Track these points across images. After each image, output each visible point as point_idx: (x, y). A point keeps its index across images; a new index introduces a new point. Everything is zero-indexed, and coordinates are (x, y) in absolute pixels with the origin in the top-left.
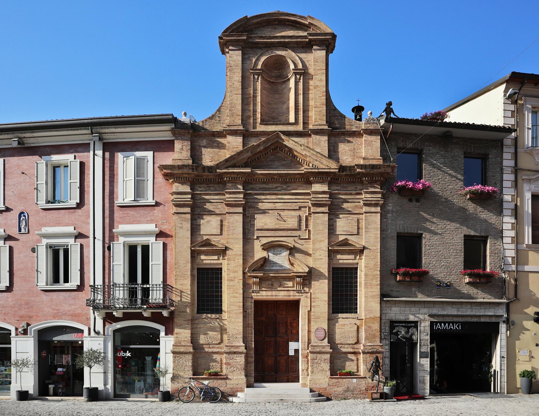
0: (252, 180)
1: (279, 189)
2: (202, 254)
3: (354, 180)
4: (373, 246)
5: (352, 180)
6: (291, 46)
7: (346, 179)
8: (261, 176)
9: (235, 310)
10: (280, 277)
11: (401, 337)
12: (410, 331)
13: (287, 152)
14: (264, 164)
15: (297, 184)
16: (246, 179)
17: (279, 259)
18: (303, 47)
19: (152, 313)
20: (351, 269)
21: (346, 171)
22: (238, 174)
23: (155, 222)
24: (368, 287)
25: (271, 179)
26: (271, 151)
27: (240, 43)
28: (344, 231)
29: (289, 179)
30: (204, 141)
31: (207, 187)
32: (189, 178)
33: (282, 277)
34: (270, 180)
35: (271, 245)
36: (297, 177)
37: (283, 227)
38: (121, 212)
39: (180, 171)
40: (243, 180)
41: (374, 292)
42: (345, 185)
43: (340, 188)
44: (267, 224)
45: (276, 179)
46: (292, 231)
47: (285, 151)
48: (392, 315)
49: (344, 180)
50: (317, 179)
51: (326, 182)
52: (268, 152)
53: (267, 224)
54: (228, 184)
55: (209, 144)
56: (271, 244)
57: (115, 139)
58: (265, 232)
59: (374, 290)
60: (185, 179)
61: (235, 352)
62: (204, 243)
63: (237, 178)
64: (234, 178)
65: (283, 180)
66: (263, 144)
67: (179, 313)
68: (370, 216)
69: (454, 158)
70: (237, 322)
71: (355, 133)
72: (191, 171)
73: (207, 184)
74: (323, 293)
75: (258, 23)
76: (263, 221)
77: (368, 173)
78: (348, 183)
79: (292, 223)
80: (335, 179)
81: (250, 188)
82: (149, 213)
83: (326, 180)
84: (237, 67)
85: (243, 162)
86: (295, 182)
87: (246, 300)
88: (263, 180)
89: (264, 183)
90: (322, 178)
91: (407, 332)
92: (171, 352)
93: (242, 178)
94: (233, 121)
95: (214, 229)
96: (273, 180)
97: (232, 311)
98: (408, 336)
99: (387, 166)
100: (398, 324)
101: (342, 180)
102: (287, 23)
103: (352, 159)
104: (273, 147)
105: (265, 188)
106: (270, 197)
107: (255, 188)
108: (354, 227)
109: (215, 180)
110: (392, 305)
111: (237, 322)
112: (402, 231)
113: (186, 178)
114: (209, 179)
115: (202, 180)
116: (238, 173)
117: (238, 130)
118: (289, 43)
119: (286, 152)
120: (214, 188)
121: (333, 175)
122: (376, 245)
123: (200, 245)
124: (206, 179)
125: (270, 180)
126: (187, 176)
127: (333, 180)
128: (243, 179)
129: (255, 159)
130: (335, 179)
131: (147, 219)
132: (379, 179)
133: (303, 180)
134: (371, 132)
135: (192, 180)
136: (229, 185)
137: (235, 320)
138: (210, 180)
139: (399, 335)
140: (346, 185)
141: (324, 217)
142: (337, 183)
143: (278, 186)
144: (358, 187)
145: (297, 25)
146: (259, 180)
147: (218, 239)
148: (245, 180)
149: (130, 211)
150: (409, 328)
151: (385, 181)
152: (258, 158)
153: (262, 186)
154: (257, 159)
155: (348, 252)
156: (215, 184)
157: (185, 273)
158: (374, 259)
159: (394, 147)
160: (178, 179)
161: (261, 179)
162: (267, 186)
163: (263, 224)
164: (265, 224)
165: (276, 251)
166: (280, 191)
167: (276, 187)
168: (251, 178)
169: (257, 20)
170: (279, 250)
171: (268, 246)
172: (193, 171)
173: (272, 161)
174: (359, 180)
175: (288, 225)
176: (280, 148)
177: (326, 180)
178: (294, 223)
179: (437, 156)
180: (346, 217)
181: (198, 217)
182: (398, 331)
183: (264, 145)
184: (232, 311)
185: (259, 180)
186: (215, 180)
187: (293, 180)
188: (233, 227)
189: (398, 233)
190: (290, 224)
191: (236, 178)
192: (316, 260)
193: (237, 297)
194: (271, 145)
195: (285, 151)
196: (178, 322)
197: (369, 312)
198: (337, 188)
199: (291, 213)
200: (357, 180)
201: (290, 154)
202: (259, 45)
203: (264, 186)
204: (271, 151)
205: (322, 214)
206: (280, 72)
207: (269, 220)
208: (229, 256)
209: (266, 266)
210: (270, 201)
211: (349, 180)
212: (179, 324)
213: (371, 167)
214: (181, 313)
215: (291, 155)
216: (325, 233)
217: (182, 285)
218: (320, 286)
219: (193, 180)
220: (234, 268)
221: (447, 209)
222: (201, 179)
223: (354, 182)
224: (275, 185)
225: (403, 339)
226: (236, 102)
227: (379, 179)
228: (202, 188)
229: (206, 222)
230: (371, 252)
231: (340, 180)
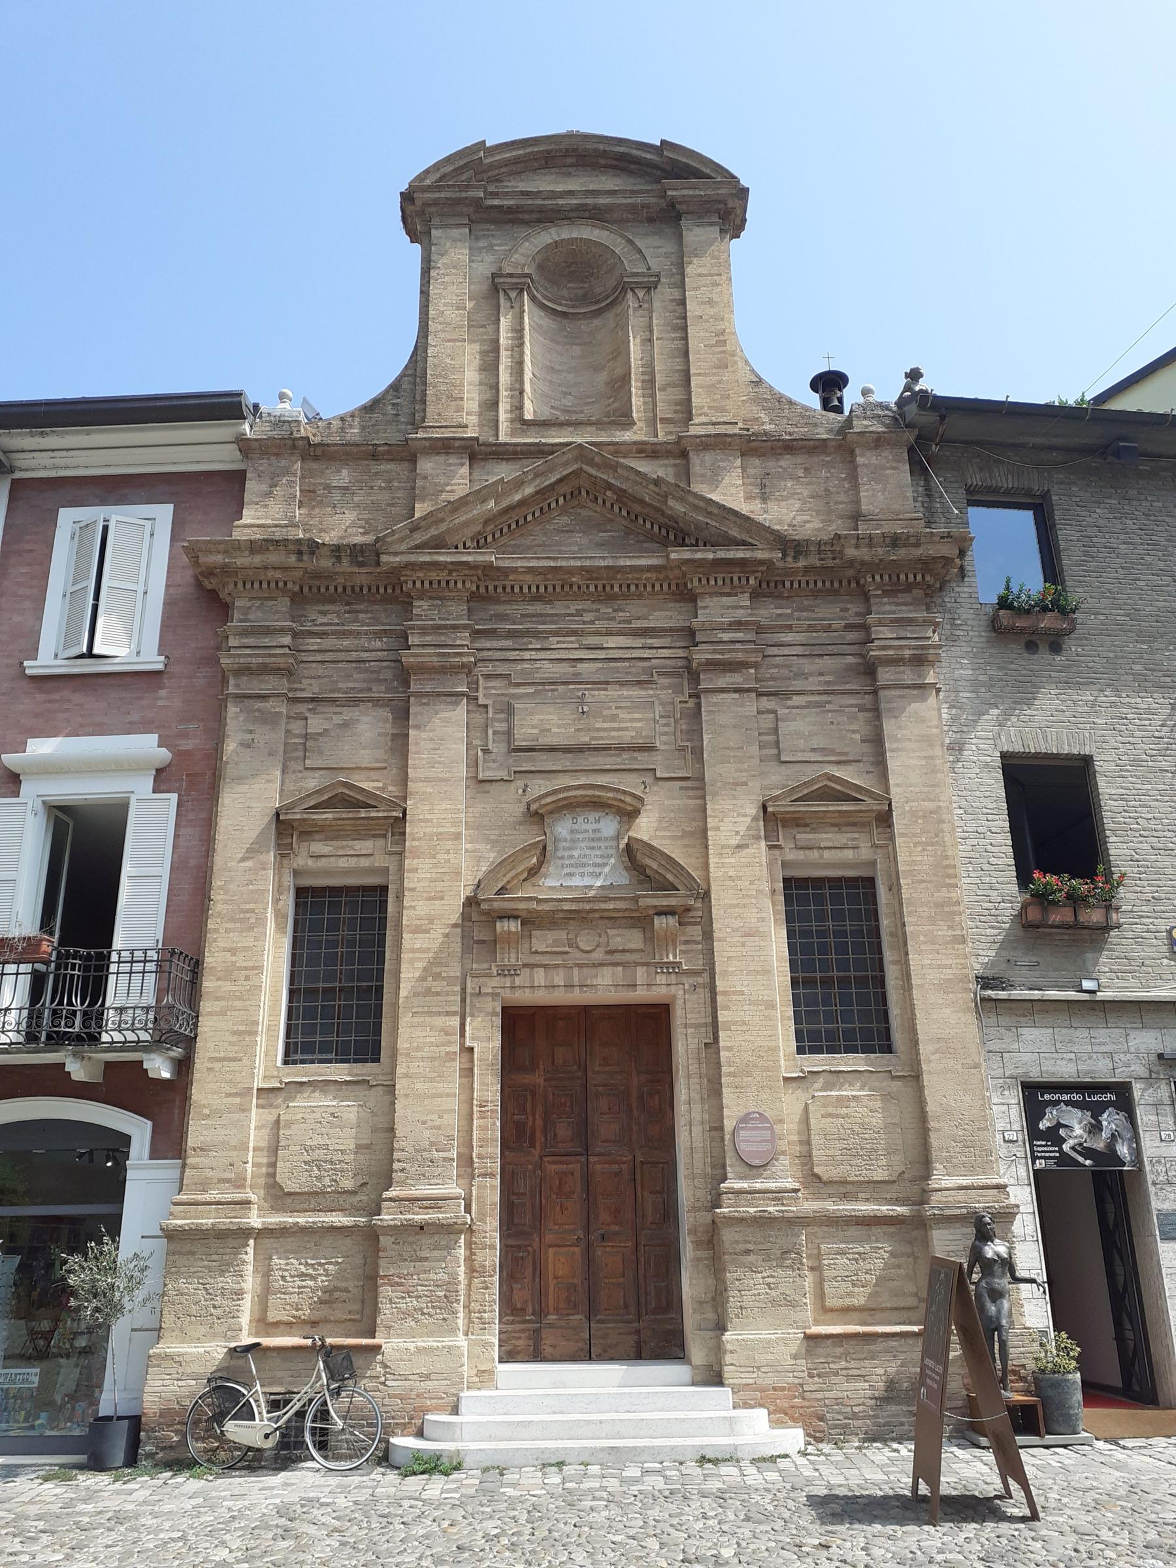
0: (500, 590)
1: (588, 617)
2: (317, 837)
3: (836, 585)
4: (923, 800)
5: (828, 584)
6: (615, 216)
7: (807, 582)
8: (529, 578)
9: (431, 1044)
10: (597, 915)
11: (1073, 1148)
12: (1105, 1123)
13: (612, 506)
14: (536, 542)
15: (647, 602)
16: (478, 587)
17: (592, 848)
18: (651, 220)
19: (108, 1065)
20: (308, 1048)
21: (806, 554)
22: (451, 571)
23: (158, 728)
24: (923, 947)
25: (562, 587)
26: (561, 500)
27: (465, 210)
28: (813, 750)
29: (620, 586)
30: (345, 472)
31: (349, 612)
32: (285, 583)
33: (606, 914)
34: (558, 589)
35: (564, 798)
36: (647, 579)
37: (602, 738)
38: (41, 697)
39: (258, 559)
40: (467, 590)
41: (946, 966)
42: (806, 603)
43: (789, 611)
44: (550, 730)
45: (579, 587)
46: (636, 754)
47: (604, 502)
48: (1027, 1058)
49: (803, 585)
50: (712, 582)
51: (742, 593)
52: (549, 505)
53: (550, 730)
54: (416, 603)
55: (358, 481)
56: (562, 796)
57: (55, 467)
58: (544, 756)
59: (944, 962)
60: (273, 585)
61: (422, 1228)
62: (326, 797)
63: (448, 582)
64: (439, 582)
65: (600, 588)
66: (533, 479)
67: (210, 1066)
68: (901, 697)
69: (1152, 518)
70: (434, 1096)
71: (826, 447)
72: (293, 559)
73: (348, 604)
74: (757, 973)
75: (516, 161)
76: (535, 722)
77: (881, 560)
78: (816, 594)
79: (635, 724)
80: (772, 585)
81: (492, 616)
82: (137, 698)
83: (742, 587)
84: (454, 271)
85: (470, 531)
86: (640, 596)
87: (473, 1006)
88: (534, 589)
89: (538, 598)
90: (728, 581)
91: (1095, 1128)
92: (160, 1233)
93: (464, 582)
94: (440, 415)
95: (364, 748)
96: (567, 588)
97: (418, 1048)
98: (1100, 1145)
99: (942, 538)
100: (1056, 1097)
101: (796, 585)
102: (602, 162)
103: (823, 521)
104: (565, 489)
105: (541, 615)
106: (558, 642)
107: (507, 615)
108: (849, 735)
109: (374, 590)
110: (1021, 1019)
111: (434, 1096)
112: (1018, 748)
113: (277, 583)
114: (353, 588)
115: (332, 589)
116: (450, 567)
117: (454, 439)
118: (609, 208)
119: (608, 504)
120: (369, 615)
121: (765, 568)
122: (932, 797)
123: (311, 804)
124: (344, 588)
125: (558, 589)
126: (278, 575)
127: (764, 585)
128: (468, 585)
129: (509, 526)
130: (772, 585)
131: (129, 718)
132: (919, 577)
133: (665, 587)
134: (878, 439)
135: (297, 588)
136: (419, 607)
137: (427, 1085)
138: (357, 589)
139: (1064, 1141)
140: (811, 603)
141: (743, 706)
142: (780, 596)
143: (585, 607)
144: (849, 606)
145: (633, 167)
146: (521, 588)
147: (380, 784)
148: (474, 588)
149: (74, 691)
150: (1096, 1110)
151: (938, 586)
152: (517, 522)
153: (531, 609)
154: (514, 526)
155: (833, 821)
156: (374, 602)
157: (251, 906)
158: (933, 844)
159: (956, 485)
160: (248, 586)
161: (530, 588)
162: (548, 610)
163: (536, 731)
164: (542, 731)
165: (580, 820)
166: (592, 622)
167: (579, 613)
168: (497, 583)
169: (514, 153)
170: (591, 819)
171: (554, 806)
172: (300, 560)
173: (563, 531)
174: (853, 585)
175: (621, 733)
176: (588, 492)
177: (742, 587)
178: (640, 724)
179: (1098, 510)
180: (817, 702)
181: (310, 710)
182: (1059, 1125)
183: (538, 481)
184: (418, 1048)
185: (521, 588)
186: (374, 590)
187: (633, 588)
188: (432, 740)
189: (1004, 756)
190: (626, 729)
191: (443, 584)
192: (724, 851)
193: (438, 994)
194: (560, 480)
195: (604, 502)
196: (204, 1102)
197: (937, 1046)
198: (779, 611)
199: (631, 693)
200: (845, 583)
201: (620, 509)
202: (520, 216)
203: (539, 608)
204: (561, 500)
205: (737, 696)
206: (586, 285)
207: (555, 717)
208: (414, 839)
209: (545, 876)
210: (558, 656)
211: (820, 584)
212: (206, 1111)
213: (888, 540)
214: (220, 1065)
215: (624, 513)
216: (750, 757)
217: (233, 951)
218: (743, 944)
219: (301, 589)
220: (432, 884)
221: (1160, 674)
222: (327, 588)
223: (834, 592)
224: (574, 607)
225: (1081, 1159)
226: (448, 361)
227: (919, 577)
228: (329, 617)
229: (340, 726)
230: (916, 822)
231: (788, 584)
